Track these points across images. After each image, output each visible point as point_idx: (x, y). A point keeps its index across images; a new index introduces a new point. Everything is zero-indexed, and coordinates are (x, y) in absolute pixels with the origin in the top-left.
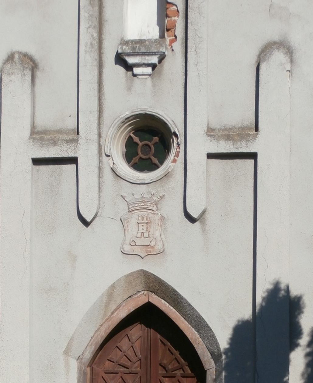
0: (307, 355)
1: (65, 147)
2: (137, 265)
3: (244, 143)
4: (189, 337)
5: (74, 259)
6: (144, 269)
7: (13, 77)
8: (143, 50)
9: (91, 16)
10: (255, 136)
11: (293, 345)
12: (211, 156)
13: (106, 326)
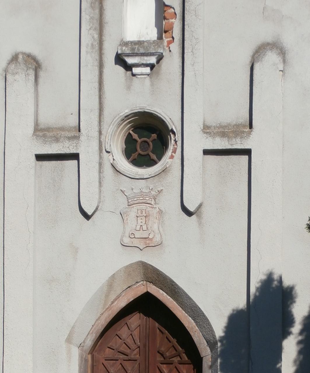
0: (299, 343)
1: (67, 143)
2: (136, 257)
3: (238, 140)
5: (76, 250)
7: (17, 77)
8: (142, 51)
9: (92, 18)
10: (249, 133)
11: (286, 334)
12: (207, 152)
13: (106, 315)
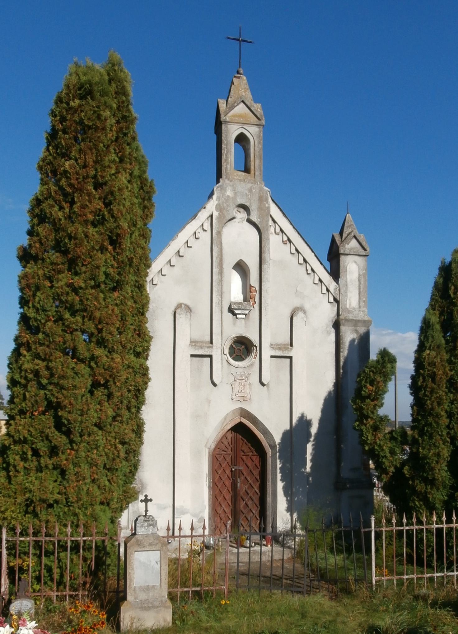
0: (313, 445)
1: (206, 350)
2: (239, 405)
3: (287, 352)
4: (259, 437)
5: (209, 402)
6: (242, 407)
7: (181, 315)
8: (243, 308)
10: (292, 349)
11: (308, 441)
12: (272, 357)
13: (221, 433)
